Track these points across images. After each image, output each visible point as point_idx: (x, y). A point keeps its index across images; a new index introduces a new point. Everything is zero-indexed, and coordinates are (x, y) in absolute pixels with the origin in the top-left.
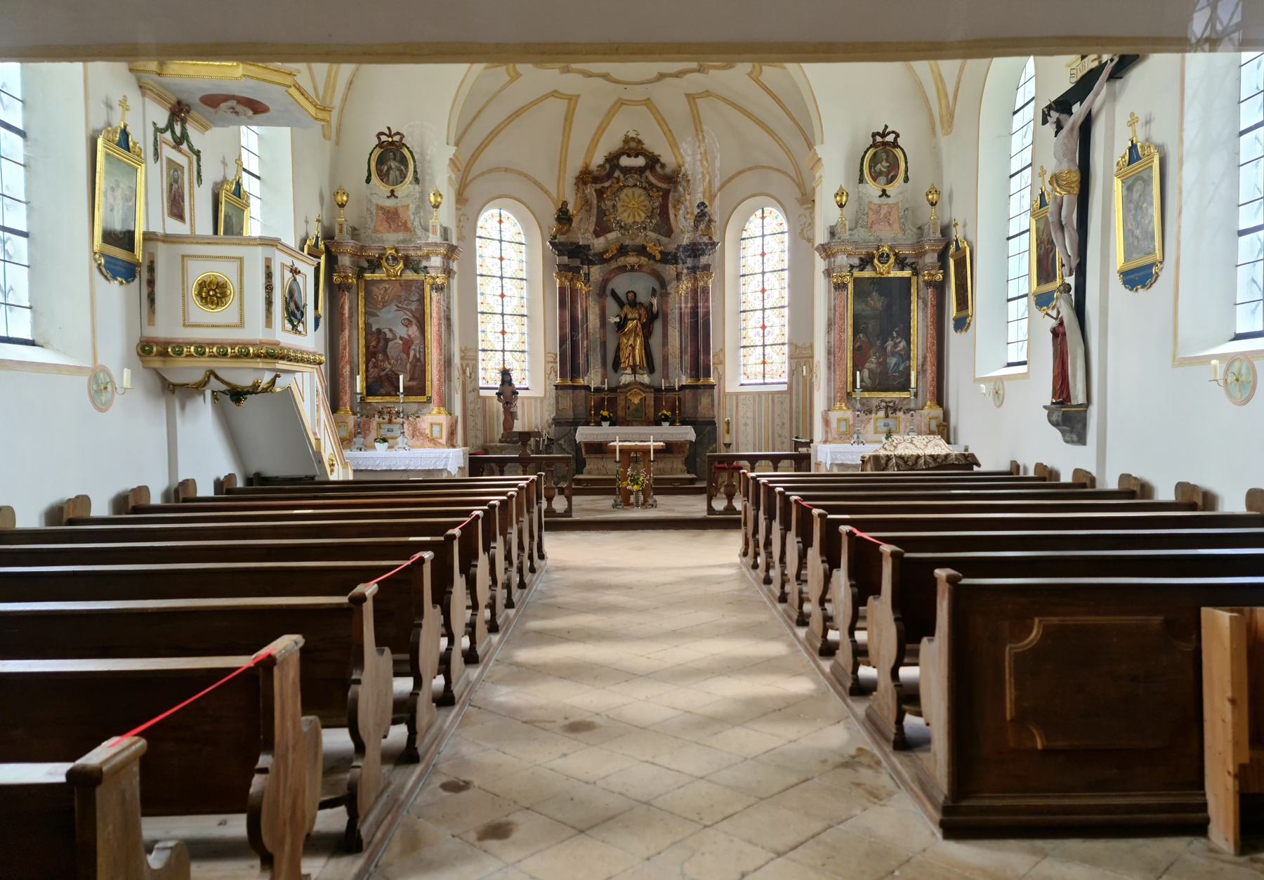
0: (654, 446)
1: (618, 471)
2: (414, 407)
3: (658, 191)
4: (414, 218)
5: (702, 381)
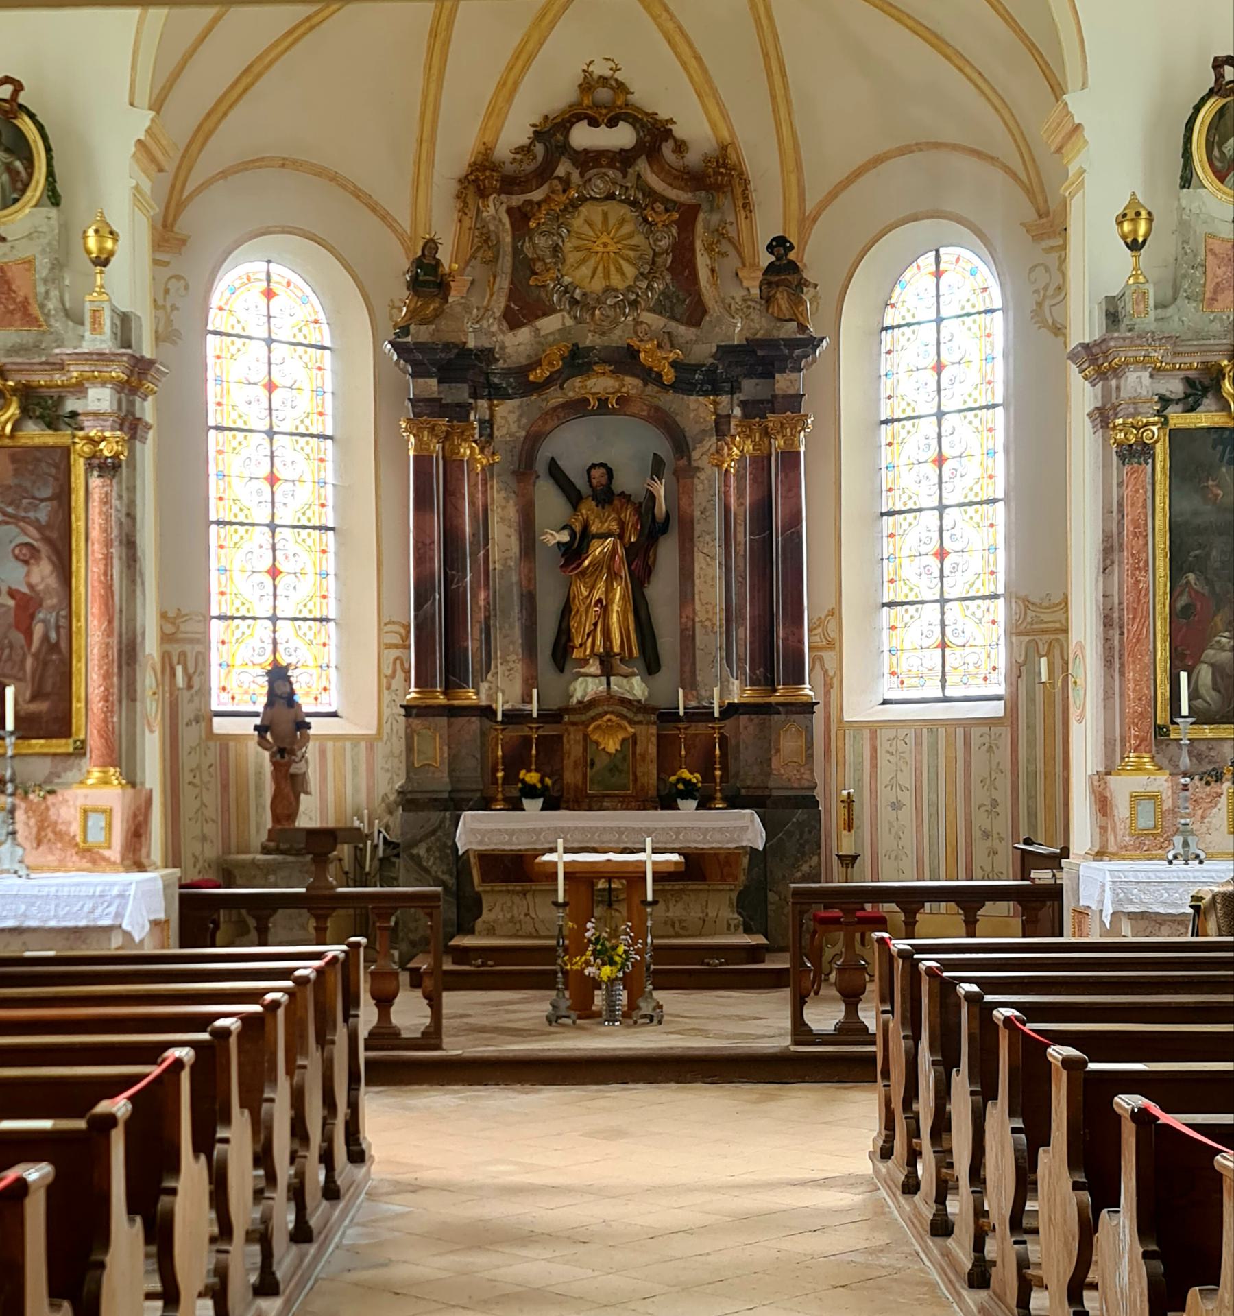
0: (654, 863)
1: (561, 928)
2: (41, 768)
3: (667, 210)
4: (47, 292)
5: (781, 694)
